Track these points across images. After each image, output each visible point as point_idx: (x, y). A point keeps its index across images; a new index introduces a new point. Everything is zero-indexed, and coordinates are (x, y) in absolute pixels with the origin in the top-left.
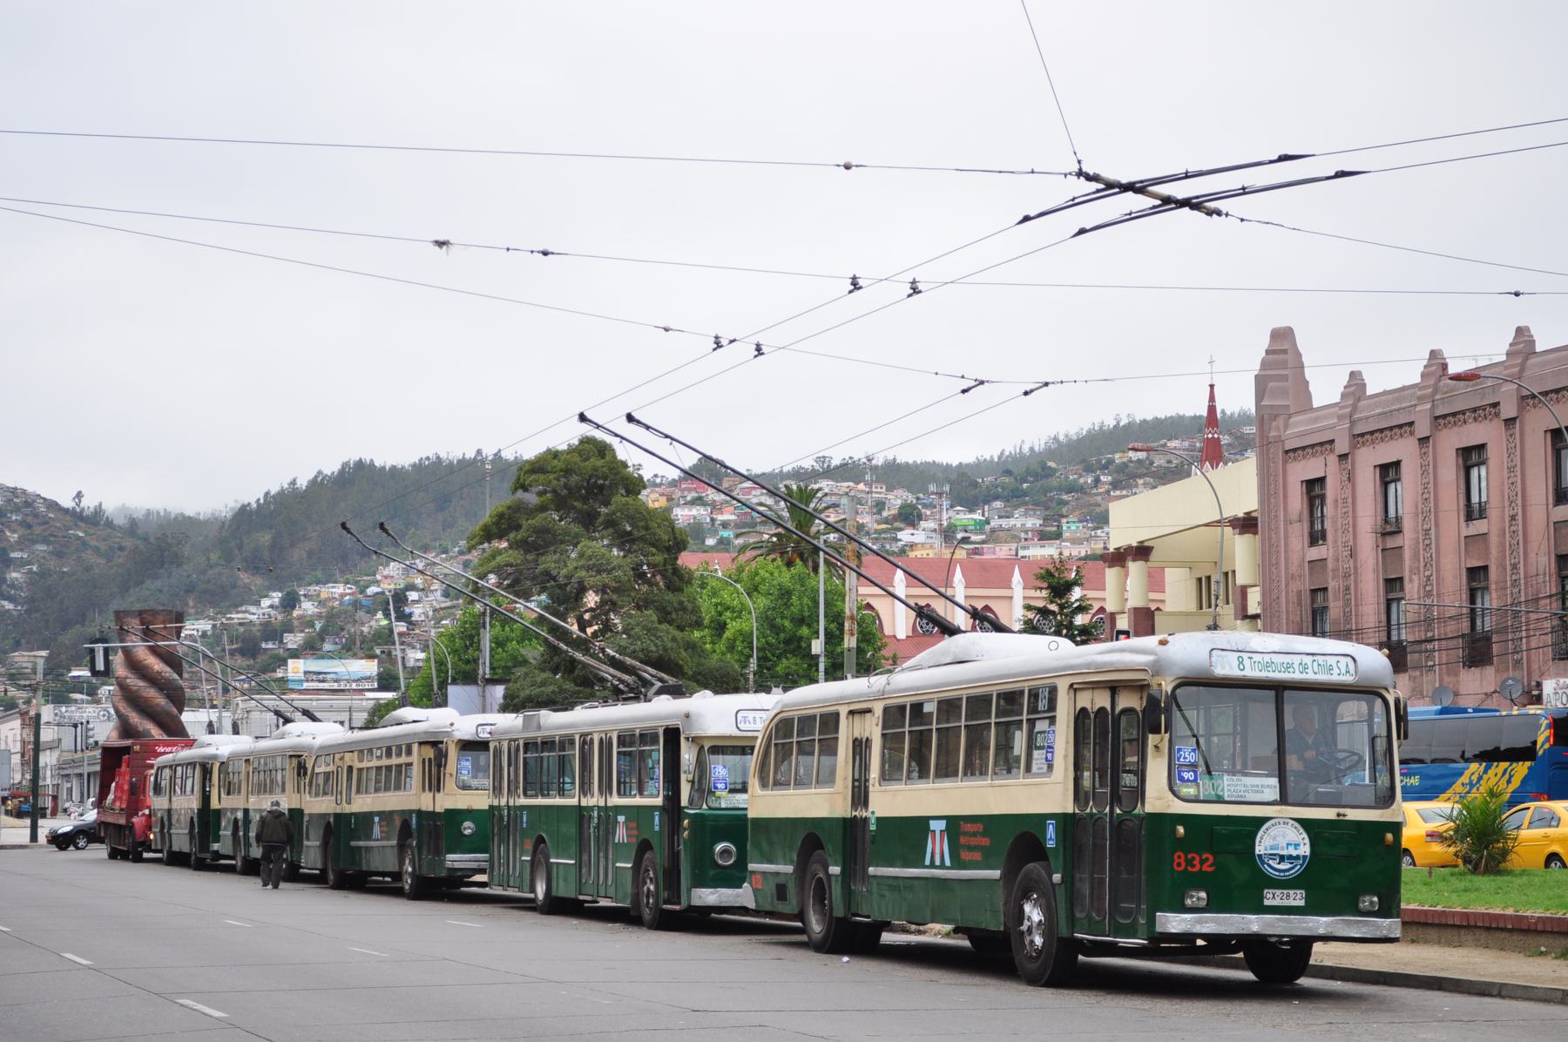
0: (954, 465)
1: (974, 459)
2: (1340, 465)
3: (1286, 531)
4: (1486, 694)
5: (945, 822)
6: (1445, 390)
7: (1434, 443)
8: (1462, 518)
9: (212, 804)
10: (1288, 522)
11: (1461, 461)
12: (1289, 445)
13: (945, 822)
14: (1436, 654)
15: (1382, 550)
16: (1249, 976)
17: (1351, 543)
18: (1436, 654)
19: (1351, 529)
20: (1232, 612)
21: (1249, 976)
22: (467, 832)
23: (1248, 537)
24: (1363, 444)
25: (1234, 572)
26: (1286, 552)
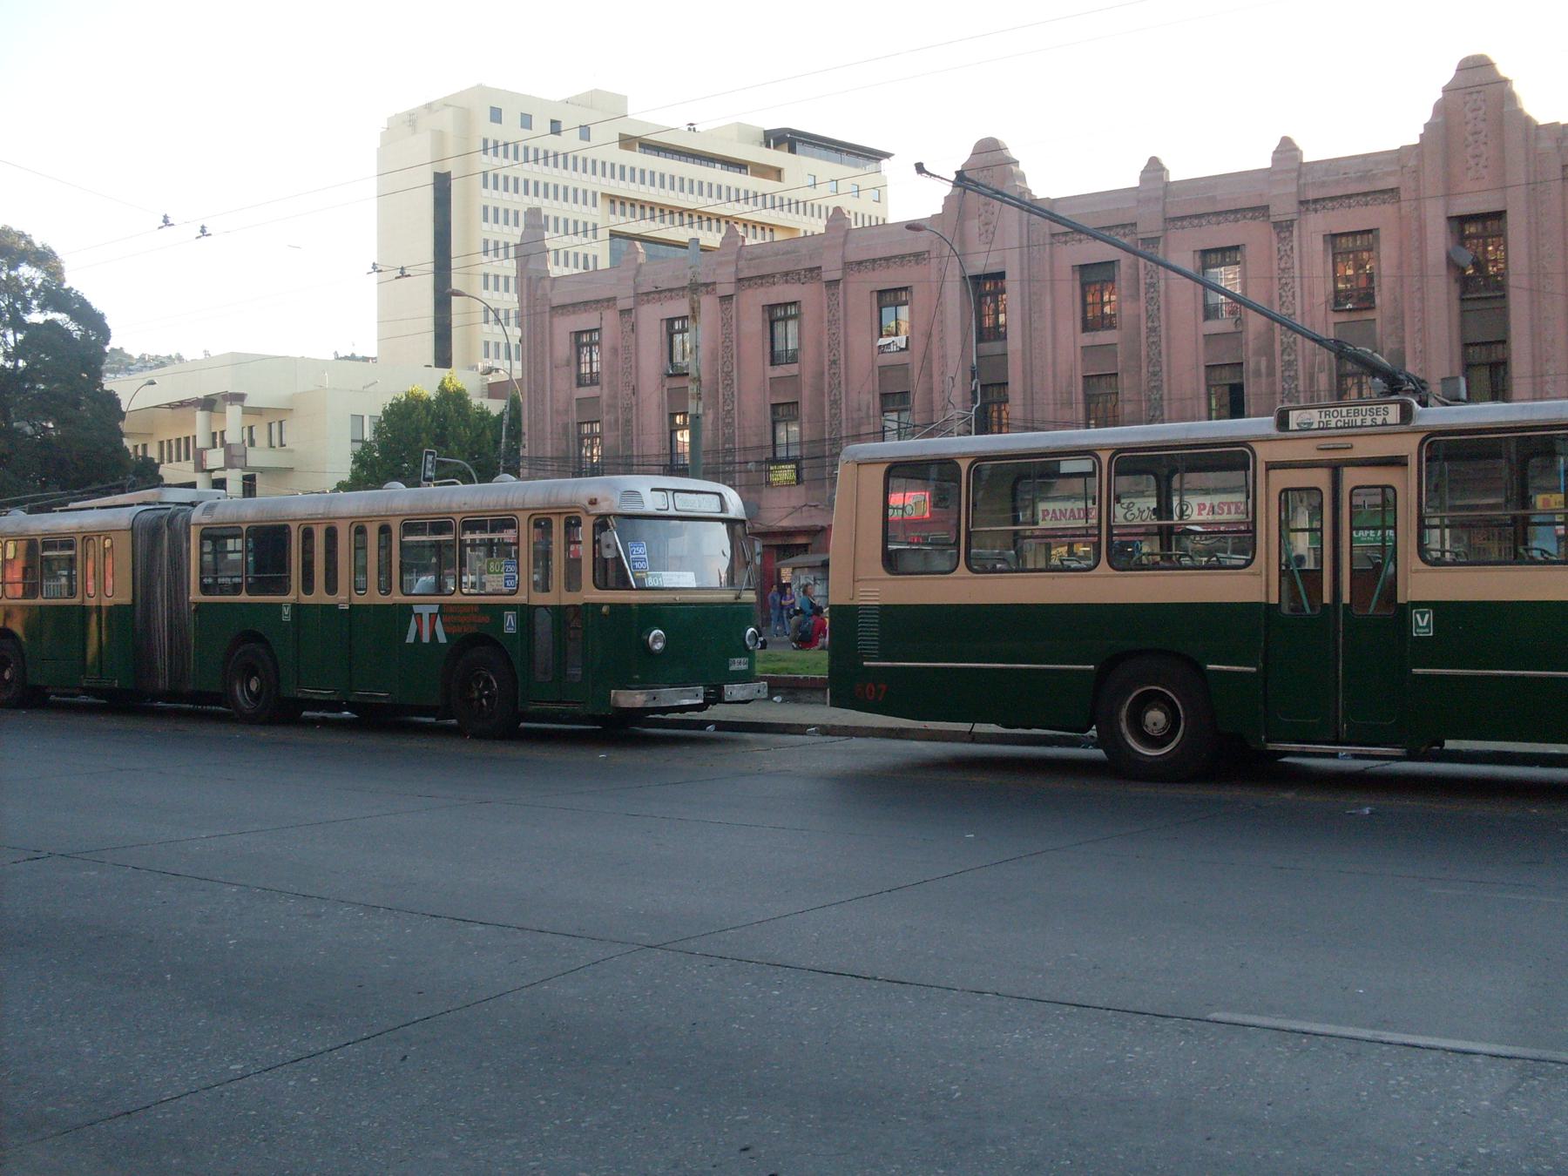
0: (1308, 157)
1: (1128, 178)
2: (621, 320)
3: (552, 374)
4: (794, 507)
5: (1277, 602)
6: (749, 257)
7: (636, 312)
8: (768, 363)
9: (1257, 596)
10: (554, 366)
11: (767, 316)
12: (555, 303)
13: (1277, 602)
14: (737, 475)
15: (668, 389)
16: (1099, 753)
17: (634, 383)
18: (737, 475)
19: (634, 371)
20: (192, 466)
21: (1099, 753)
22: (659, 646)
23: (205, 413)
24: (648, 302)
25: (195, 437)
26: (551, 390)
